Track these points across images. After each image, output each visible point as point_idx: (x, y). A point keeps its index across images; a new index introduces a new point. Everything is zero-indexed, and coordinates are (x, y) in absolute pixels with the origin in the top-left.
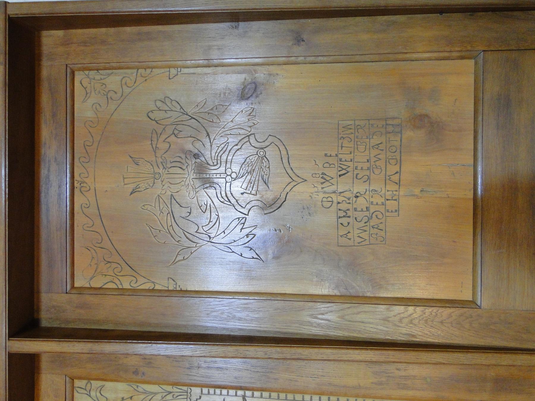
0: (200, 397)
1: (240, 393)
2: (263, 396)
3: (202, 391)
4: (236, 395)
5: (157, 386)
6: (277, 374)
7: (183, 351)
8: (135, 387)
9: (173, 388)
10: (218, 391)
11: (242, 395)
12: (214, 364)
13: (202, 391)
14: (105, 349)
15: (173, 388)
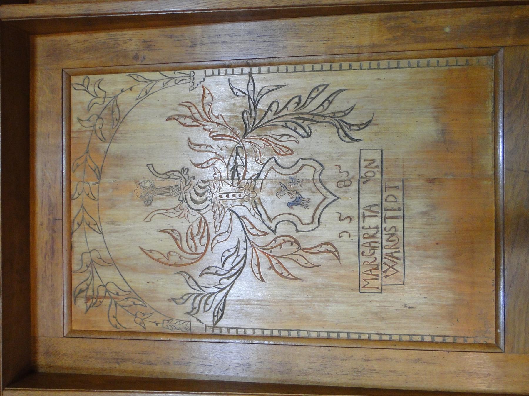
0: (204, 80)
1: (246, 70)
2: (271, 71)
3: (205, 73)
4: (242, 73)
5: (158, 73)
6: (285, 42)
7: (185, 4)
8: (135, 77)
9: (175, 73)
10: (222, 71)
11: (248, 72)
12: (218, 39)
13: (205, 73)
14: (103, 8)
15: (175, 73)
